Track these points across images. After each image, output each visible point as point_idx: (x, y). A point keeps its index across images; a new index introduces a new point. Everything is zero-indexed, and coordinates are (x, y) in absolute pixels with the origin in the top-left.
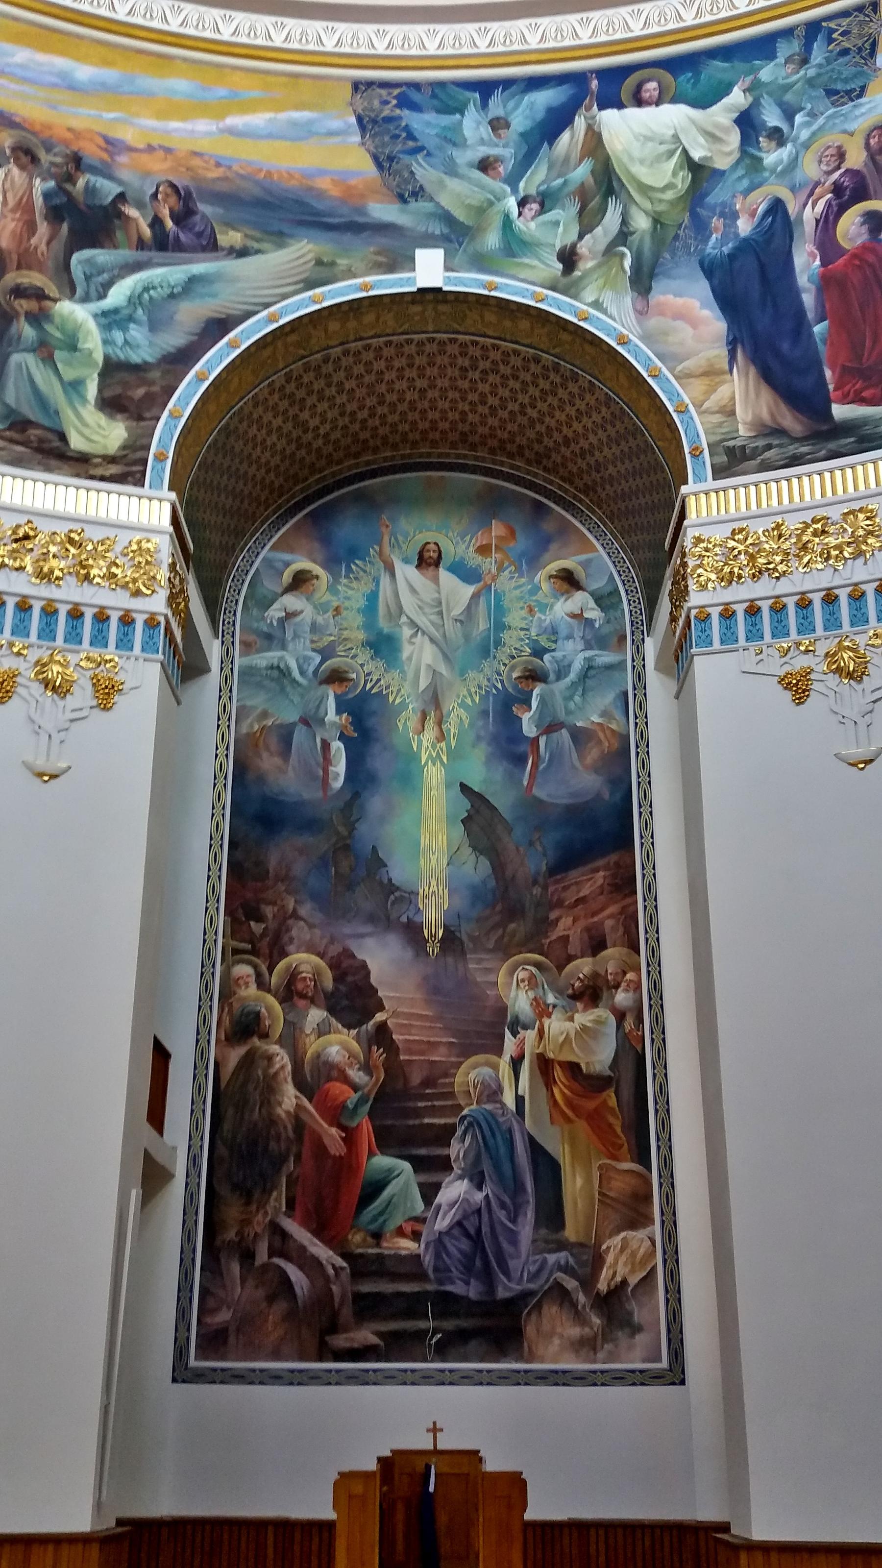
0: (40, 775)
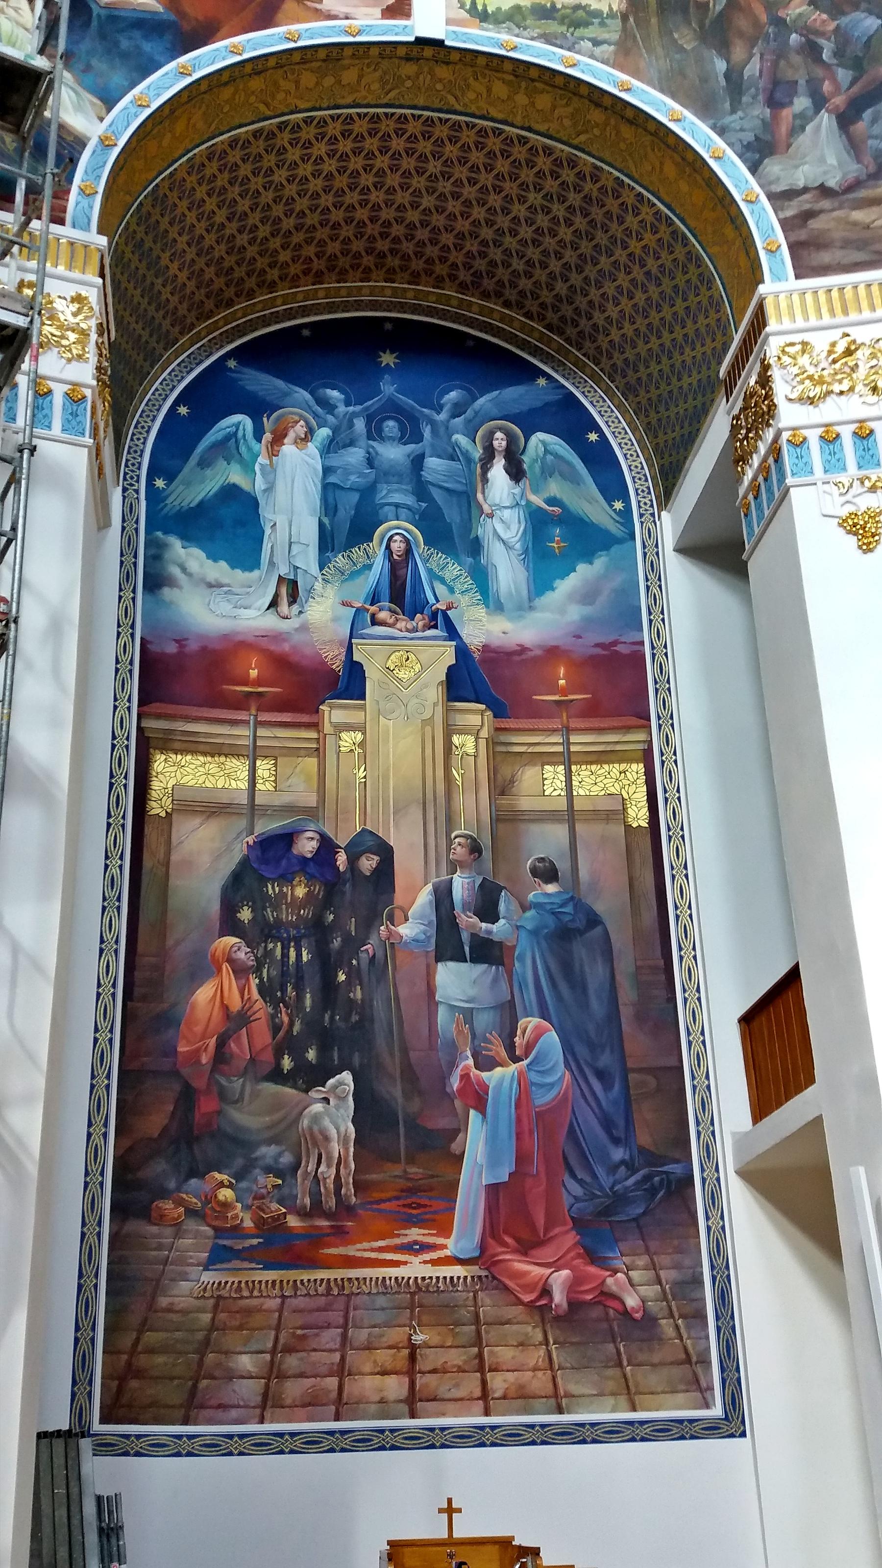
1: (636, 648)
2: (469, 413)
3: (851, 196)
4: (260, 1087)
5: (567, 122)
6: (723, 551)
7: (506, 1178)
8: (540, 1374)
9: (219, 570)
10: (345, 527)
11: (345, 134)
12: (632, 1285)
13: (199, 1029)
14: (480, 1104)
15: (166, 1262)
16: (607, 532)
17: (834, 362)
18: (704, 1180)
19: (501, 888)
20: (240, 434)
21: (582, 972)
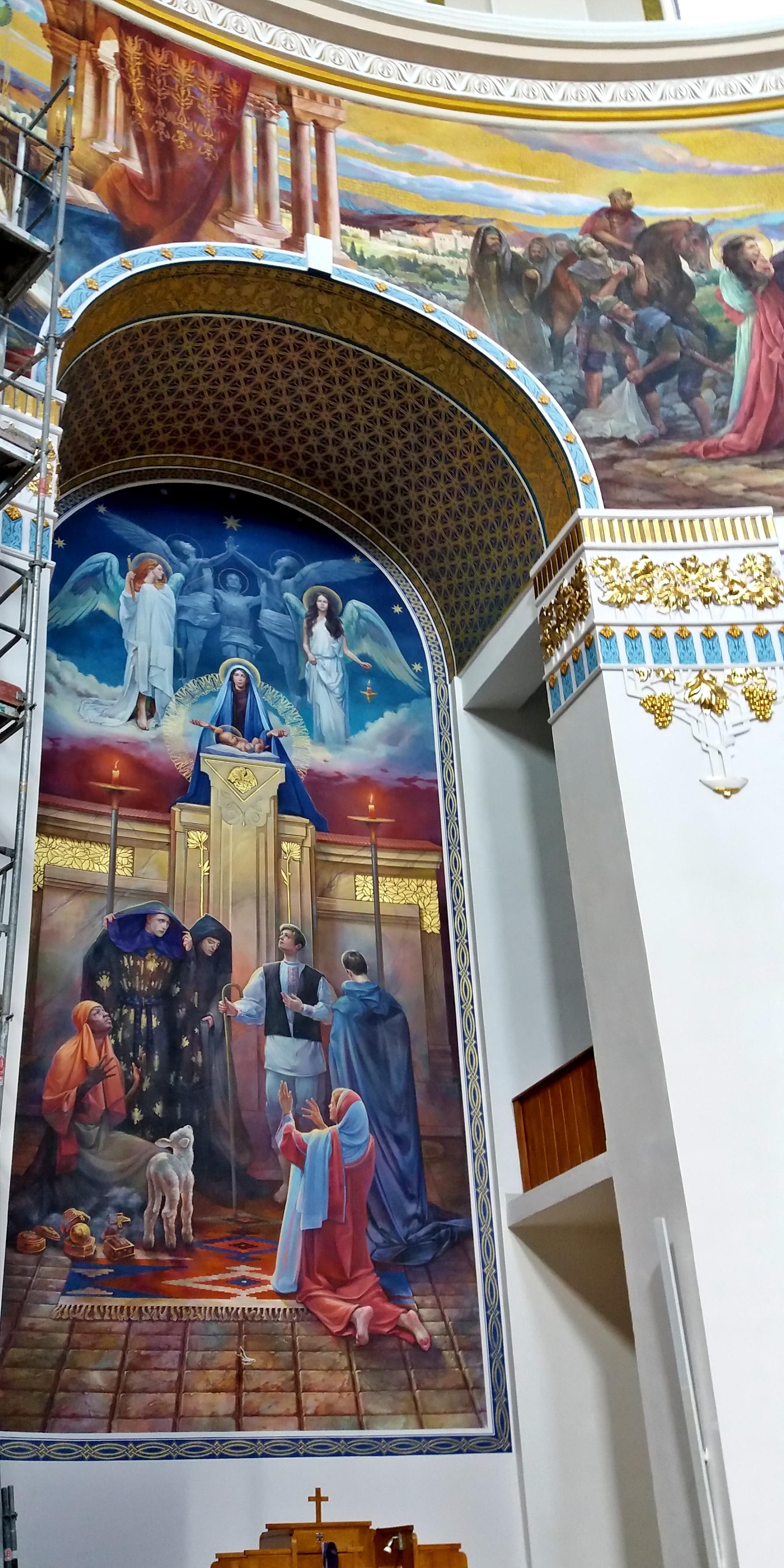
0: (718, 792)
1: (431, 785)
2: (298, 576)
3: (647, 449)
4: (113, 1135)
5: (418, 356)
6: (525, 715)
7: (320, 1226)
8: (345, 1395)
9: (88, 682)
10: (196, 658)
11: (232, 336)
12: (422, 1321)
13: (61, 1081)
14: (300, 1161)
15: (28, 1286)
16: (408, 688)
17: (636, 576)
18: (481, 1234)
19: (320, 976)
20: (108, 569)
21: (385, 1054)
